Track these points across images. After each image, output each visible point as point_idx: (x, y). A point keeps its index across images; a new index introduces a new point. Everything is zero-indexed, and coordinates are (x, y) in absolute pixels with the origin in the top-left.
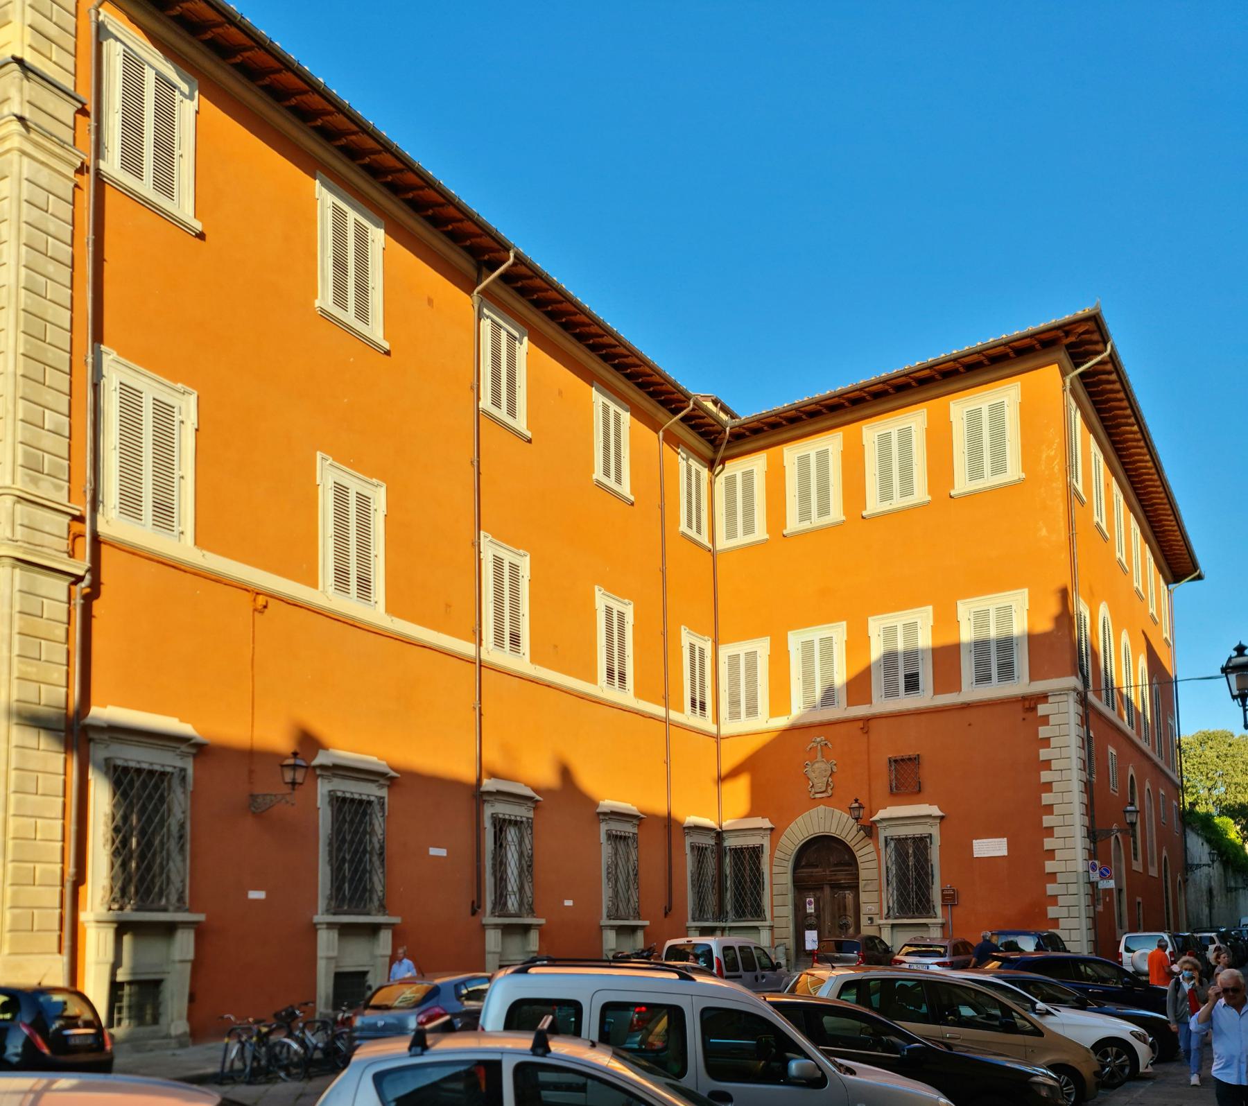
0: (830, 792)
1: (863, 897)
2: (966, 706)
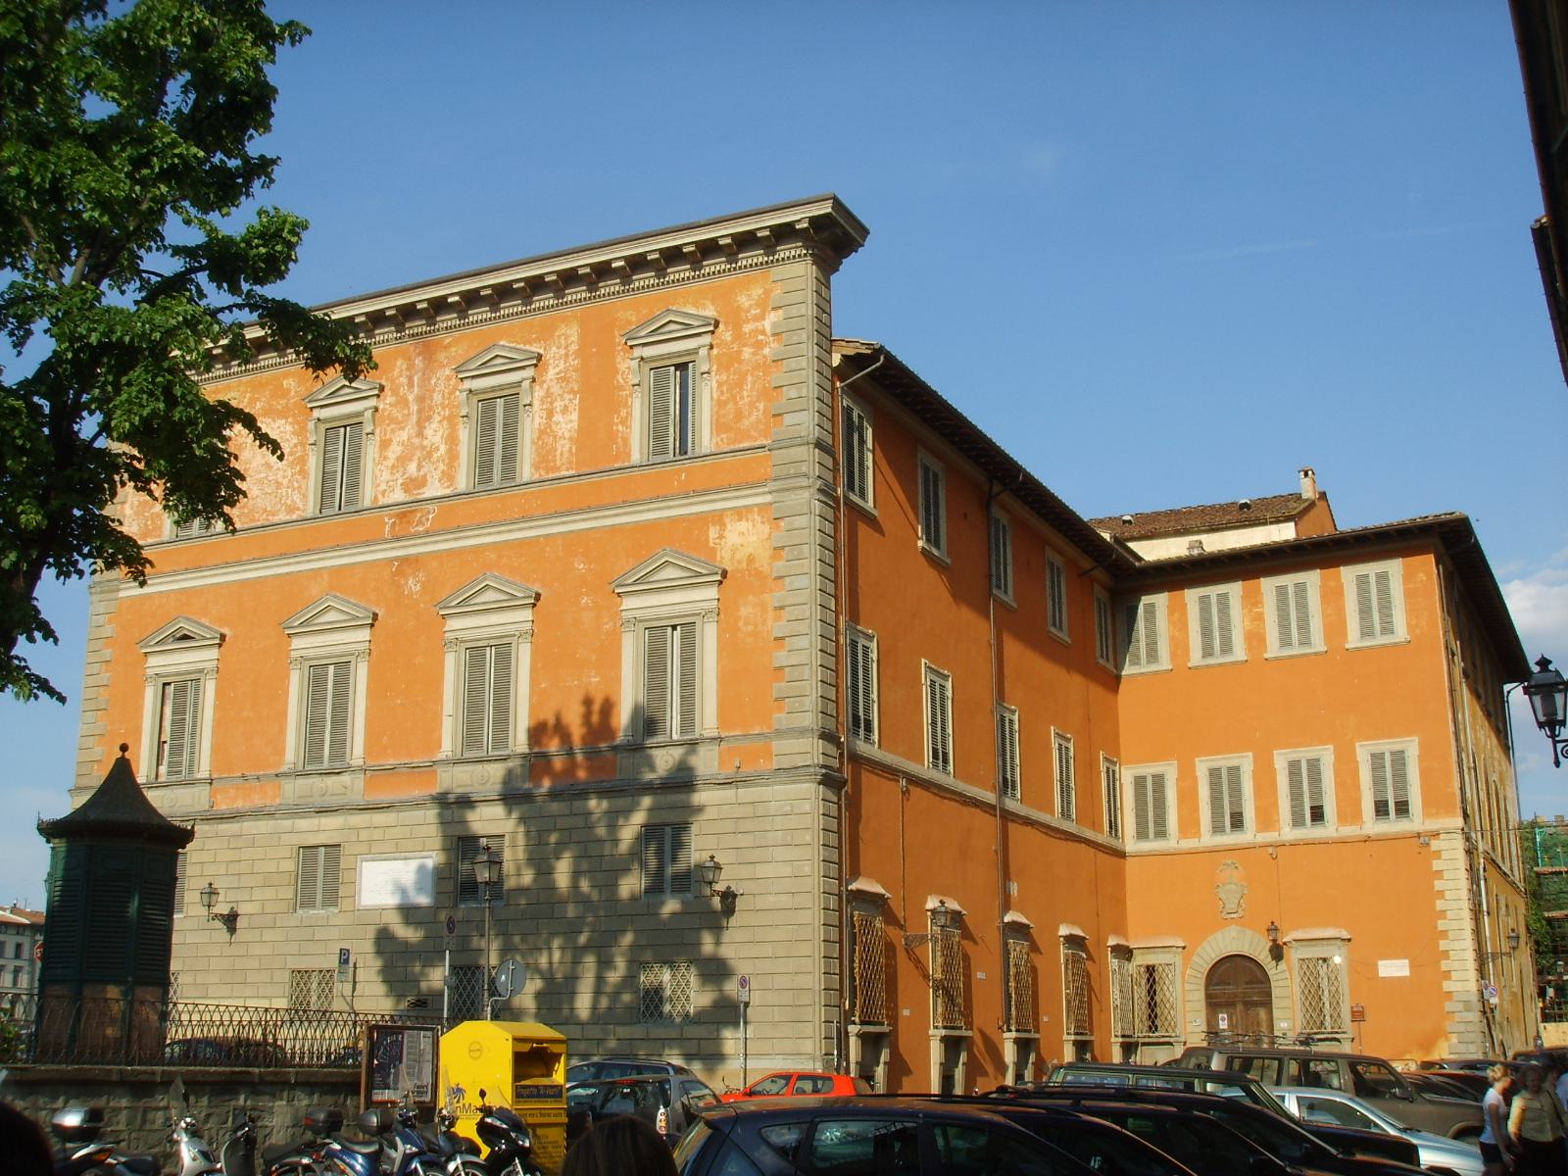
0: (1241, 913)
2: (1367, 839)
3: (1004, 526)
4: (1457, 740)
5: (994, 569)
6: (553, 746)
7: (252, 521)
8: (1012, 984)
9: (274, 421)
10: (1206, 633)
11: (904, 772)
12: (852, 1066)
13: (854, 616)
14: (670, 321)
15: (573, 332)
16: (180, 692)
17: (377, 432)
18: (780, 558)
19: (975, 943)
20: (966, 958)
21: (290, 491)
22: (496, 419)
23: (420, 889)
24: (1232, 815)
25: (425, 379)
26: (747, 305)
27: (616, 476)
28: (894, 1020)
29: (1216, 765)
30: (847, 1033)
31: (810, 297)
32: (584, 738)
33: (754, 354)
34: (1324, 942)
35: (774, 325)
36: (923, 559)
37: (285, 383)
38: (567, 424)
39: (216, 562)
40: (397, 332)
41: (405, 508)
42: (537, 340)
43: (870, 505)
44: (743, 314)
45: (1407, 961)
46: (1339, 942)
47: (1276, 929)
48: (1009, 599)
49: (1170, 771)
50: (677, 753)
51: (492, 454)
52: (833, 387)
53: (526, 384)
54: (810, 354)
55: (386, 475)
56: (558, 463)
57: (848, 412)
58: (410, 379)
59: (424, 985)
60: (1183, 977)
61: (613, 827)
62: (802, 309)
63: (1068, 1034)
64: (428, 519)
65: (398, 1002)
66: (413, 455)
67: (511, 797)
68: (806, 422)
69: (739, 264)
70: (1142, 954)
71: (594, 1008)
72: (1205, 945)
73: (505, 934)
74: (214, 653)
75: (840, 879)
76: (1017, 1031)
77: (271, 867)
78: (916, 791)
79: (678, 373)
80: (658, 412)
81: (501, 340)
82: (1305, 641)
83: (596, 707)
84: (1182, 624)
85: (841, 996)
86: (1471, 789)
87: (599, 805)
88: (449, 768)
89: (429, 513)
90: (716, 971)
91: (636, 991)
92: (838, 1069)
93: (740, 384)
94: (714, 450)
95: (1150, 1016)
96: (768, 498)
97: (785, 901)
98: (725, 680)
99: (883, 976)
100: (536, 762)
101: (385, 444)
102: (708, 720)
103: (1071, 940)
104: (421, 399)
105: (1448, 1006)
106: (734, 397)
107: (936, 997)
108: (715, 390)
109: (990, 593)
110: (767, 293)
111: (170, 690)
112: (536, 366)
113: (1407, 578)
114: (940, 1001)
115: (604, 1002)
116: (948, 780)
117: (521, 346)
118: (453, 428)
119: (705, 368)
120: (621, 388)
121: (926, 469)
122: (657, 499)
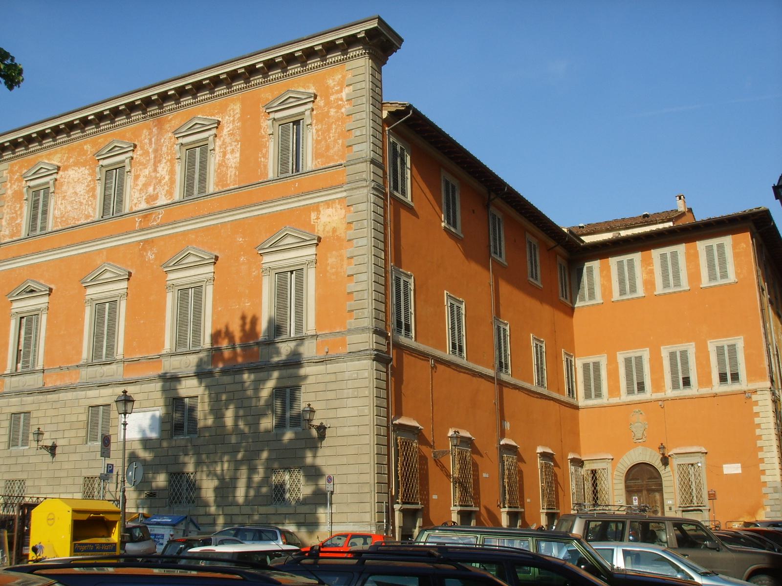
0: (644, 439)
1: (665, 496)
2: (715, 395)
3: (499, 219)
4: (766, 338)
5: (492, 243)
6: (224, 344)
7: (67, 224)
8: (506, 480)
9: (79, 168)
10: (622, 282)
11: (432, 356)
12: (397, 529)
13: (398, 262)
14: (290, 97)
15: (236, 108)
16: (28, 321)
17: (133, 171)
18: (350, 229)
19: (482, 456)
20: (475, 465)
21: (87, 206)
22: (196, 159)
23: (152, 428)
24: (638, 384)
25: (158, 140)
26: (332, 85)
27: (258, 187)
28: (426, 501)
29: (628, 355)
30: (393, 510)
31: (368, 77)
32: (241, 339)
33: (337, 112)
34: (692, 455)
35: (347, 95)
36: (445, 233)
37: (85, 147)
38: (234, 159)
39: (48, 249)
40: (143, 114)
41: (144, 213)
42: (218, 113)
43: (409, 199)
44: (330, 90)
45: (740, 465)
46: (700, 454)
47: (664, 448)
48: (503, 260)
49: (603, 360)
50: (292, 345)
51: (193, 179)
52: (384, 130)
53: (211, 138)
54: (368, 110)
55: (137, 195)
56: (228, 182)
57: (393, 146)
58: (150, 140)
59: (154, 485)
60: (612, 476)
61: (257, 390)
62: (363, 85)
63: (543, 509)
64: (159, 218)
65: (140, 495)
66: (151, 182)
67: (201, 374)
68: (365, 149)
69: (328, 61)
70: (589, 463)
71: (246, 496)
72: (624, 457)
73: (198, 454)
74: (46, 299)
75: (388, 417)
76: (509, 507)
77: (74, 418)
78: (441, 368)
79: (295, 127)
80: (283, 150)
81: (199, 114)
82: (677, 283)
83: (248, 320)
84: (607, 276)
85: (389, 487)
86: (776, 367)
87: (249, 377)
88: (168, 359)
89: (159, 214)
90: (314, 474)
91: (271, 486)
92: (386, 531)
93: (329, 130)
94: (314, 169)
95: (594, 498)
96: (344, 194)
97: (353, 431)
98: (319, 301)
99: (518, 485)
100: (215, 353)
101: (137, 177)
102: (310, 325)
103: (544, 455)
104: (156, 151)
105: (764, 490)
106: (325, 138)
107: (455, 488)
108: (314, 134)
109: (490, 255)
110: (344, 77)
111: (24, 321)
112: (217, 127)
113: (734, 247)
114: (457, 490)
115: (252, 493)
116: (463, 362)
117: (210, 117)
118: (172, 166)
119: (309, 122)
120: (263, 137)
121: (447, 183)
122: (284, 198)
